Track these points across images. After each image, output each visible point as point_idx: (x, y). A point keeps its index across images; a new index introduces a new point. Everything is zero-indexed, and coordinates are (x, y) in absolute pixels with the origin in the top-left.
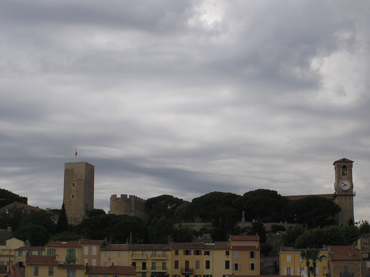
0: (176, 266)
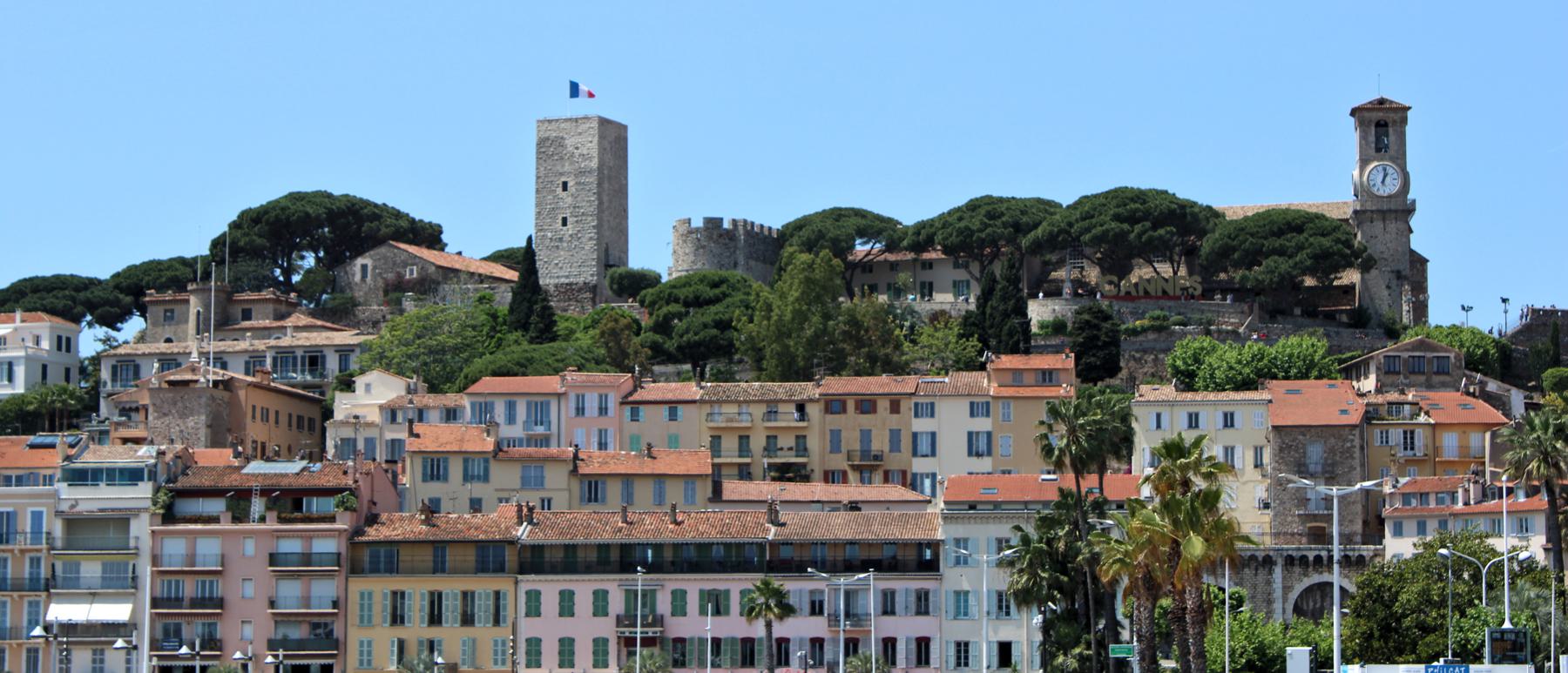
0: (835, 447)
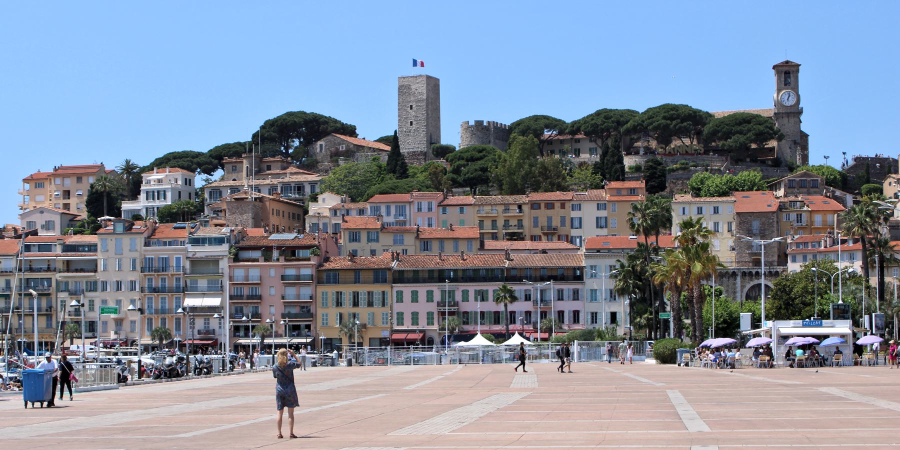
0: (536, 224)
